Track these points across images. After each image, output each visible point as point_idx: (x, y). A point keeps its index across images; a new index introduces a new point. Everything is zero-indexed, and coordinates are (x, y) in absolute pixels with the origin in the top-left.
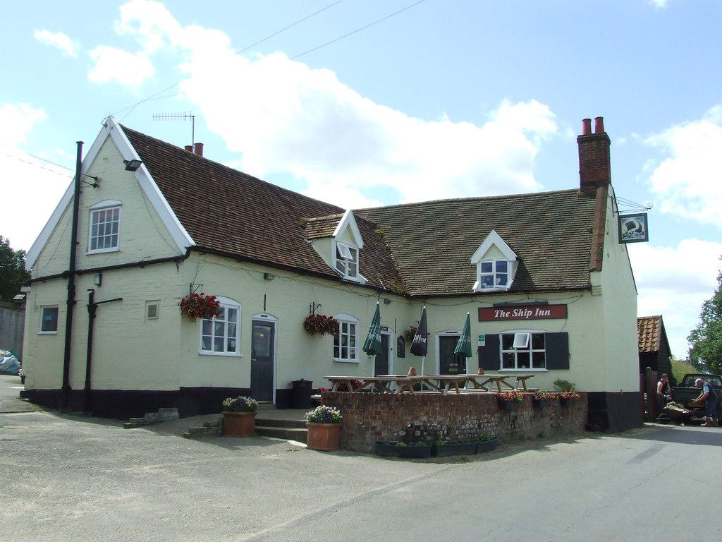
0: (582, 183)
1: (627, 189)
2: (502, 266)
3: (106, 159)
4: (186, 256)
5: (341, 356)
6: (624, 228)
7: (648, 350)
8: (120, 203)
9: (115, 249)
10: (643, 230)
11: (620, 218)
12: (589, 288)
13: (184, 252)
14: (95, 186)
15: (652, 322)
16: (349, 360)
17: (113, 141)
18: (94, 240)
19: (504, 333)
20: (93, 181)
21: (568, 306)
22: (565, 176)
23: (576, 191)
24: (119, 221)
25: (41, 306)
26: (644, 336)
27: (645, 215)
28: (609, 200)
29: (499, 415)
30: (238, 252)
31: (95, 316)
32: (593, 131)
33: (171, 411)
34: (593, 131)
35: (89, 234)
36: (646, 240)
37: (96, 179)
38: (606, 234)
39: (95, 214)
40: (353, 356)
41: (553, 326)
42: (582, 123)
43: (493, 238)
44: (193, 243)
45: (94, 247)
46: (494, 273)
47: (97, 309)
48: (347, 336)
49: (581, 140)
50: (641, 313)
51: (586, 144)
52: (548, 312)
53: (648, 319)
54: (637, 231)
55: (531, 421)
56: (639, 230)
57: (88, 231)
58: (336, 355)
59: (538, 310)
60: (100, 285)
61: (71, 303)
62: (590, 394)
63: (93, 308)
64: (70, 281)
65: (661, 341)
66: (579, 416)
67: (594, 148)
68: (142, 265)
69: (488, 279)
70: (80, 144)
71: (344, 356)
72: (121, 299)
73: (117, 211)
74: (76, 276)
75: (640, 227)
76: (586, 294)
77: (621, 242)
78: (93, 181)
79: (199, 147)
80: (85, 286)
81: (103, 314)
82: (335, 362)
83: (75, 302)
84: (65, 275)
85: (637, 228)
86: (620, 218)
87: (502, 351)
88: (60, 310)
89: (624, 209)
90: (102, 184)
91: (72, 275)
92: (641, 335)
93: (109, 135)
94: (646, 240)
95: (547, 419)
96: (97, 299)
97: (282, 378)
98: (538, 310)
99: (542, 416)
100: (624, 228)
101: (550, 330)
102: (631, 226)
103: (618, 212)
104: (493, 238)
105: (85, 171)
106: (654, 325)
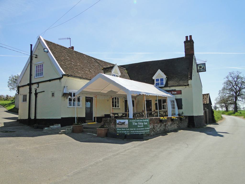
0: (186, 55)
1: (199, 56)
2: (162, 80)
3: (39, 49)
4: (62, 77)
5: (114, 107)
6: (198, 68)
7: (206, 103)
8: (43, 62)
9: (42, 76)
10: (204, 68)
11: (197, 65)
12: (188, 85)
13: (62, 76)
14: (36, 57)
15: (206, 95)
16: (117, 108)
17: (41, 44)
18: (36, 74)
19: (163, 99)
20: (35, 56)
21: (182, 91)
22: (181, 54)
23: (184, 57)
24: (43, 68)
25: (22, 94)
26: (204, 99)
27: (205, 64)
28: (194, 59)
29: (160, 124)
30: (80, 76)
31: (37, 97)
32: (189, 40)
33: (58, 125)
34: (189, 40)
35: (35, 72)
36: (205, 71)
37: (36, 55)
38: (193, 69)
39: (37, 66)
40: (118, 107)
41: (179, 96)
42: (185, 37)
43: (159, 71)
44: (64, 73)
45: (36, 76)
46: (159, 82)
47: (38, 95)
48: (116, 101)
49: (185, 42)
50: (203, 93)
51: (187, 43)
52: (176, 93)
53: (205, 95)
54: (202, 69)
55: (171, 125)
56: (203, 68)
57: (35, 71)
58: (113, 106)
59: (173, 92)
60: (38, 87)
61: (30, 93)
62: (189, 116)
63: (36, 94)
64: (30, 86)
65: (209, 101)
66: (186, 124)
67: (189, 44)
68: (50, 81)
69: (158, 84)
70: (31, 45)
71: (116, 106)
72: (44, 91)
73: (42, 65)
74: (31, 85)
75: (203, 67)
76: (187, 87)
77: (198, 72)
78: (35, 56)
79: (73, 48)
80: (34, 87)
81: (39, 95)
82: (113, 108)
83: (31, 93)
84: (28, 85)
85: (202, 67)
86: (197, 65)
87: (162, 104)
88: (27, 95)
89: (198, 62)
90: (38, 57)
91: (30, 84)
92: (203, 99)
93: (40, 42)
94: (205, 71)
95: (175, 125)
96: (37, 92)
97: (96, 114)
98: (173, 92)
99: (174, 124)
100: (198, 68)
101: (55, 59)
102: (200, 67)
103: (196, 63)
104: (159, 71)
105: (33, 53)
106: (207, 96)
